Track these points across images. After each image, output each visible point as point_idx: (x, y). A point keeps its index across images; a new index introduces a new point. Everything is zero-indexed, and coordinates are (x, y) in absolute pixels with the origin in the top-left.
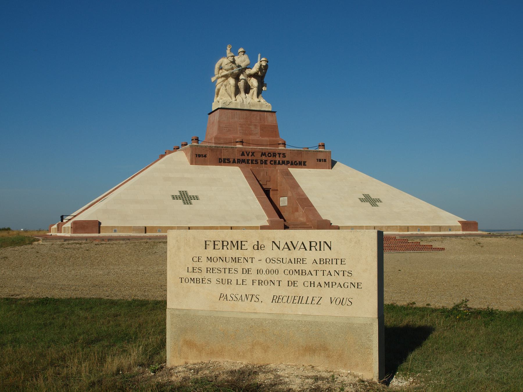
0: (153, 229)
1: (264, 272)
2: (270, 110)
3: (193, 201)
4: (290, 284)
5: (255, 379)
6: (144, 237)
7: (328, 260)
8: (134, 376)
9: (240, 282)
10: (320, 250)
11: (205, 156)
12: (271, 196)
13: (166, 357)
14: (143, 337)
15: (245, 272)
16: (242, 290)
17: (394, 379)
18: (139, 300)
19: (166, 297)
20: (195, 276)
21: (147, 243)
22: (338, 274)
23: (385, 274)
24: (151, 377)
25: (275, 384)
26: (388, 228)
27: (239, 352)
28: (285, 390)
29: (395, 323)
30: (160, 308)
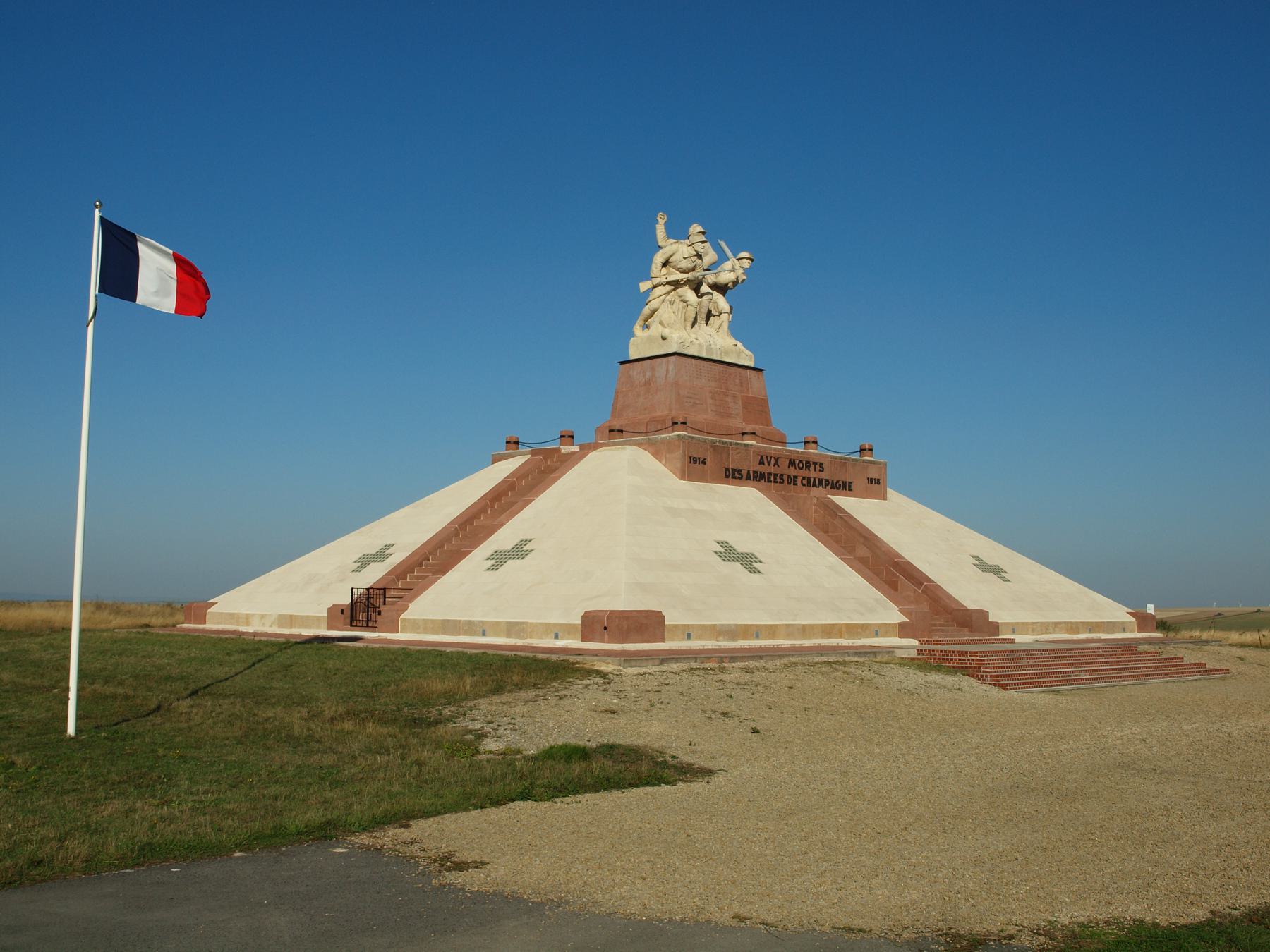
2: (751, 364)
11: (704, 463)
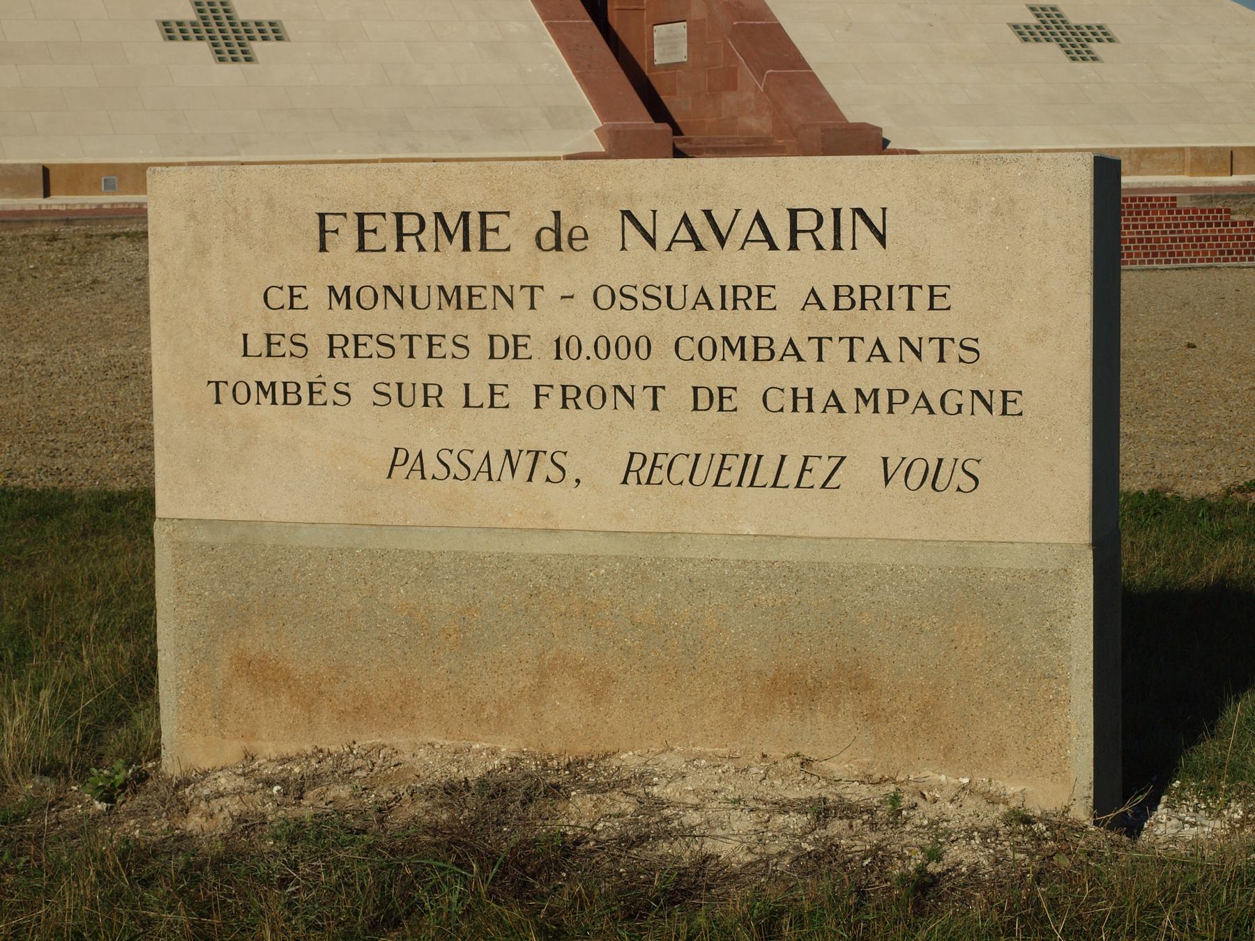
0: (80, 176)
1: (588, 350)
3: (257, 47)
4: (703, 402)
5: (553, 816)
6: (40, 212)
7: (871, 293)
8: (17, 819)
9: (480, 394)
10: (837, 247)
12: (614, 18)
13: (158, 734)
14: (54, 650)
15: (499, 351)
16: (487, 433)
17: (1161, 812)
18: (30, 493)
19: (150, 477)
20: (280, 371)
21: (54, 238)
22: (918, 354)
23: (1126, 364)
24: (95, 820)
25: (642, 839)
26: (1145, 157)
27: (481, 705)
28: (686, 861)
29: (1169, 571)
30: (125, 526)
